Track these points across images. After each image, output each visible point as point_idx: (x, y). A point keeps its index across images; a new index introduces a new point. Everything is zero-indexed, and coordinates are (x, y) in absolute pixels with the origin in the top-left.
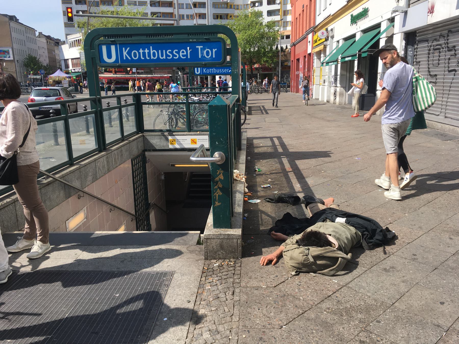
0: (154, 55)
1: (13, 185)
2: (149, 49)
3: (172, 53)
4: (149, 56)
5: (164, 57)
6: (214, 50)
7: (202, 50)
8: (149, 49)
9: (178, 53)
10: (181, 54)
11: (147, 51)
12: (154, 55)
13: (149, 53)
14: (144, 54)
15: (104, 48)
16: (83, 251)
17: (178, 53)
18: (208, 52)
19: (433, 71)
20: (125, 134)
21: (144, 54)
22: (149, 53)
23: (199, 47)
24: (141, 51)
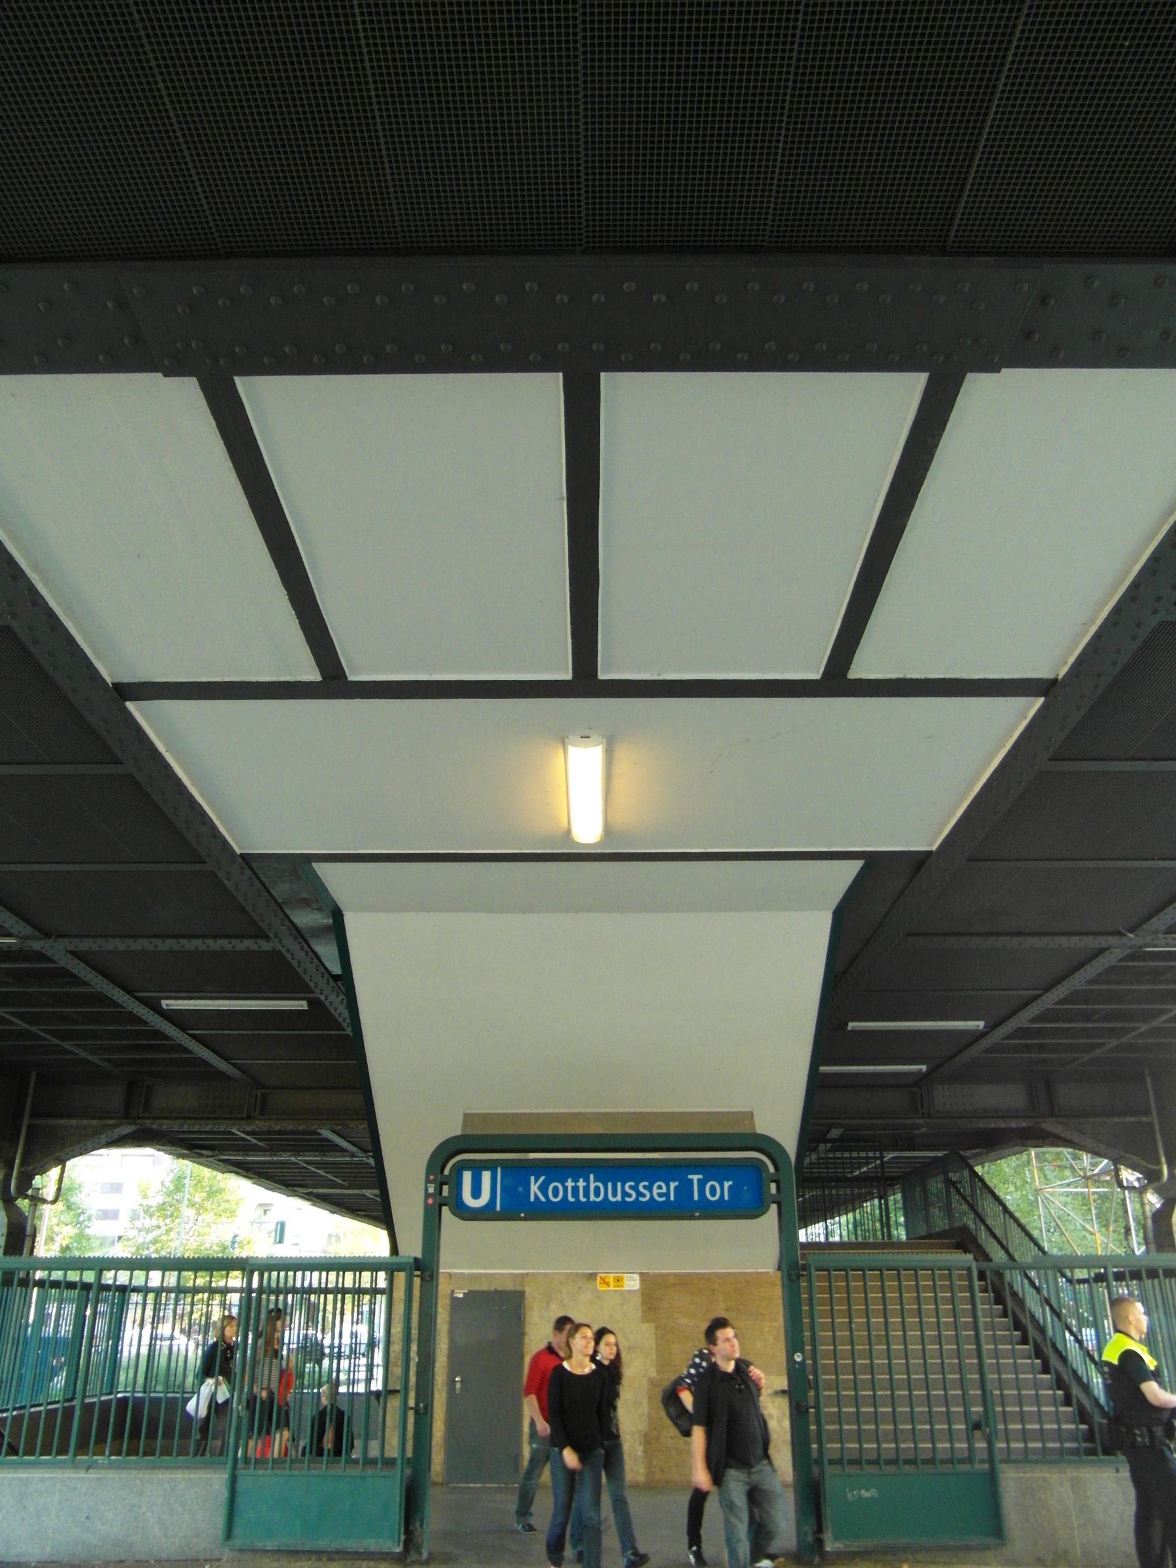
0: (597, 1194)
2: (587, 1180)
3: (640, 1194)
4: (587, 1194)
5: (619, 1198)
6: (727, 1184)
7: (702, 1184)
9: (649, 1188)
10: (655, 1191)
11: (581, 1184)
12: (597, 1194)
13: (587, 1189)
14: (575, 1189)
15: (467, 1176)
17: (649, 1188)
18: (556, 1190)
20: (312, 674)
21: (575, 1189)
22: (587, 1189)
23: (695, 1178)
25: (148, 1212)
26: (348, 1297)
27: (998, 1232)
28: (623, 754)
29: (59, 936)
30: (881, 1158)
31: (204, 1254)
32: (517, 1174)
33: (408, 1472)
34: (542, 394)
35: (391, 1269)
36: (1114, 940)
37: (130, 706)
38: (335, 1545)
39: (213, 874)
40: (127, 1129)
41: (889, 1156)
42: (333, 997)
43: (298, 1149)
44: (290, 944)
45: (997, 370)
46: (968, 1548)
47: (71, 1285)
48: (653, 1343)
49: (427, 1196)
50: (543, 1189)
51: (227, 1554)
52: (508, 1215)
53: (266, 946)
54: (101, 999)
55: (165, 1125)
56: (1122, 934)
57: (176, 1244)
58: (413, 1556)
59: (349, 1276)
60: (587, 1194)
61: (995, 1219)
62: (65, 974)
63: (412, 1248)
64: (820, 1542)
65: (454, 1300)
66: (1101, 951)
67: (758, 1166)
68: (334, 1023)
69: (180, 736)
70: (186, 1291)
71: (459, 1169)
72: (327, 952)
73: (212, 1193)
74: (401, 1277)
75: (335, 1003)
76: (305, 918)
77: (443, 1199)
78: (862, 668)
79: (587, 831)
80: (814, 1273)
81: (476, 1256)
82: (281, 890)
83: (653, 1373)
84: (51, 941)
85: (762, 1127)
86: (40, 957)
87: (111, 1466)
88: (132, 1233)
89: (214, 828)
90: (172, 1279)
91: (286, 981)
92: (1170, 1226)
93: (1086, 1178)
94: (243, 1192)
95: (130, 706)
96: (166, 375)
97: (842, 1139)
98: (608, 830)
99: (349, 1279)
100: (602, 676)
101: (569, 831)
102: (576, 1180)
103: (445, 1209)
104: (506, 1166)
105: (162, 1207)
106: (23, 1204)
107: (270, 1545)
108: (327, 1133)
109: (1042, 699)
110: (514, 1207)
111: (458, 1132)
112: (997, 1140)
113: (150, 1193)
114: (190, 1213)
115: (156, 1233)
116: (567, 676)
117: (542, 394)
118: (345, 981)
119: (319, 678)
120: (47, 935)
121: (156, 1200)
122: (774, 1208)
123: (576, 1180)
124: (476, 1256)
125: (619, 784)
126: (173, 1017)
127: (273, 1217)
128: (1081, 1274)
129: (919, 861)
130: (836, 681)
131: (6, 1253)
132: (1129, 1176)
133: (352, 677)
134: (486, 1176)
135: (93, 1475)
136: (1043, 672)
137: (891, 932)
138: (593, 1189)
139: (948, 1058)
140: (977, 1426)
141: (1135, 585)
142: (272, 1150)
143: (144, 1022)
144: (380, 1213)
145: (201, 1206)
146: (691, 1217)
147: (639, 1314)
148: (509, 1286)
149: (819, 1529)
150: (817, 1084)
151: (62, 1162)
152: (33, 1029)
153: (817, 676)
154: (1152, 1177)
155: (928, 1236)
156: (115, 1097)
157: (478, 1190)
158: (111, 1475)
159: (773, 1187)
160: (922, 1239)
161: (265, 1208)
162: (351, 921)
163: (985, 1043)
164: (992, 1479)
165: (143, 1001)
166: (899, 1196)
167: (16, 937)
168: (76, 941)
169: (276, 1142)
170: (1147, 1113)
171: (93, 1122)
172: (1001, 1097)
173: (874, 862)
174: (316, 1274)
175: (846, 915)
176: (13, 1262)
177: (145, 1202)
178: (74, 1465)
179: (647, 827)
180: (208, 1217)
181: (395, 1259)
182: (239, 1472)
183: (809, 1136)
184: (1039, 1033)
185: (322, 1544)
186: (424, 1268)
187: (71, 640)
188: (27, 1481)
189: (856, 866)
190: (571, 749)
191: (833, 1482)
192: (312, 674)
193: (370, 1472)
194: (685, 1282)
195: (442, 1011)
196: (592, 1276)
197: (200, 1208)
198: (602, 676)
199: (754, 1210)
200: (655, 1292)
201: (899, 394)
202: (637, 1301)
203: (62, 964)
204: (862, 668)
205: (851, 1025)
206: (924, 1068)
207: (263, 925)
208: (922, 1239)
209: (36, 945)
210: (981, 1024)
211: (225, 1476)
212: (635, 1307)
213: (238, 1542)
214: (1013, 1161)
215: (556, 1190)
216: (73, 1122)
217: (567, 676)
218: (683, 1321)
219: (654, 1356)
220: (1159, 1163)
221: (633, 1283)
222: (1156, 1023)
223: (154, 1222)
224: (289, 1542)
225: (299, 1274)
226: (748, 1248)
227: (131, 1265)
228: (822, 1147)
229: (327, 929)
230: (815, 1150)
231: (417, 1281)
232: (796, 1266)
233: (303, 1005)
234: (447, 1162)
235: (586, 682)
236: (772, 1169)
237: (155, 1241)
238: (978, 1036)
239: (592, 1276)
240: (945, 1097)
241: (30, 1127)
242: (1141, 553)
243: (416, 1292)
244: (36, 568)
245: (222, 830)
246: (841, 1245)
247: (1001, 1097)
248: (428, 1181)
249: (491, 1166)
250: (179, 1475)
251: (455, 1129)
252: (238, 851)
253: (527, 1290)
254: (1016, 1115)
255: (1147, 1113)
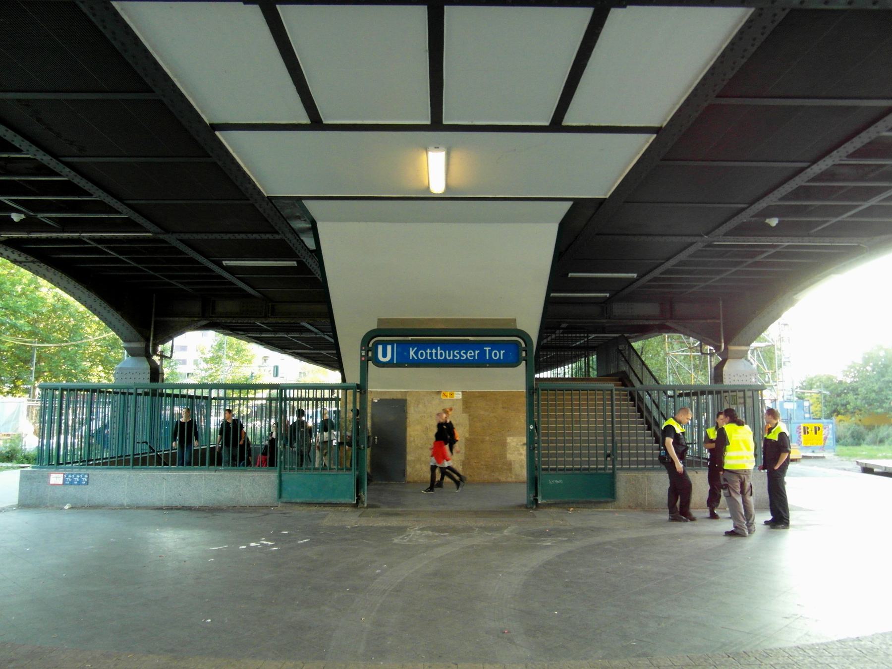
0: (441, 355)
1: (570, 275)
2: (436, 349)
3: (461, 356)
4: (436, 356)
6: (502, 352)
7: (490, 352)
8: (436, 349)
9: (466, 353)
11: (434, 351)
12: (441, 355)
13: (436, 354)
14: (431, 354)
15: (380, 348)
16: (780, 316)
17: (466, 353)
18: (422, 354)
19: (219, 406)
20: (307, 121)
21: (431, 354)
22: (436, 354)
23: (487, 349)
24: (428, 351)
25: (205, 360)
26: (319, 403)
27: (639, 375)
28: (456, 157)
29: (174, 232)
30: (588, 337)
31: (237, 382)
32: (403, 347)
33: (357, 473)
34: (420, 13)
35: (345, 389)
36: (697, 239)
37: (217, 133)
38: (327, 501)
39: (253, 205)
40: (204, 323)
41: (592, 336)
42: (310, 260)
43: (288, 331)
44: (290, 236)
45: (624, 6)
46: (600, 502)
47: (184, 396)
48: (467, 422)
49: (362, 356)
50: (416, 353)
51: (280, 504)
52: (399, 365)
53: (277, 237)
54: (192, 260)
55: (223, 320)
56: (701, 236)
57: (222, 377)
58: (360, 505)
59: (319, 392)
60: (436, 356)
61: (637, 368)
62: (174, 250)
63: (354, 378)
64: (536, 500)
65: (373, 403)
66: (692, 244)
67: (517, 344)
68: (310, 272)
69: (242, 148)
70: (229, 399)
71: (377, 343)
72: (310, 243)
73: (238, 352)
74: (350, 392)
75: (312, 263)
76: (298, 225)
77: (369, 357)
78: (568, 121)
79: (438, 187)
80: (540, 392)
81: (384, 383)
82: (286, 212)
83: (467, 435)
84: (170, 235)
85: (520, 326)
86: (163, 241)
87: (225, 470)
88: (198, 372)
89: (255, 185)
90: (222, 393)
91: (285, 251)
92: (722, 371)
93: (690, 348)
94: (256, 351)
95: (217, 133)
96: (245, 3)
97: (567, 328)
98: (447, 186)
99: (327, 393)
100: (445, 122)
101: (428, 188)
102: (431, 350)
103: (370, 362)
104: (398, 342)
105: (212, 359)
106: (156, 358)
107: (298, 501)
108: (304, 324)
109: (655, 136)
110: (402, 362)
111: (375, 327)
112: (644, 331)
113: (206, 351)
114: (228, 361)
115: (210, 372)
116: (428, 122)
117: (416, 17)
118: (317, 253)
119: (309, 122)
120: (167, 231)
121: (209, 355)
122: (524, 362)
123: (431, 350)
124: (384, 383)
125: (454, 168)
126: (231, 270)
127: (271, 363)
128: (670, 393)
129: (601, 202)
130: (556, 125)
131: (151, 381)
132: (708, 348)
133: (325, 122)
134: (389, 348)
135: (218, 473)
136: (656, 124)
137: (586, 236)
138: (439, 353)
139: (620, 291)
140: (609, 456)
141: (696, 89)
142: (275, 331)
143: (213, 271)
144: (335, 362)
145: (233, 358)
146: (486, 367)
147: (461, 409)
148: (399, 397)
149: (536, 495)
150: (549, 302)
151: (171, 338)
152: (139, 266)
153: (547, 123)
154: (717, 348)
155: (607, 376)
156: (197, 308)
157: (386, 354)
158: (226, 473)
159: (524, 354)
160: (604, 376)
161: (265, 359)
162: (320, 226)
163: (635, 285)
164: (612, 476)
165: (213, 262)
166: (595, 357)
167: (152, 233)
168: (182, 235)
169: (277, 328)
170: (719, 319)
171: (187, 319)
172: (649, 309)
173: (578, 203)
174: (311, 391)
175: (564, 227)
176: (155, 385)
177: (203, 356)
178: (209, 470)
179: (464, 181)
180: (237, 364)
181: (344, 384)
182: (283, 473)
183: (546, 326)
184: (664, 279)
185: (321, 500)
186: (361, 388)
187: (191, 106)
188: (190, 476)
189: (570, 204)
190: (430, 153)
191: (543, 478)
192: (307, 121)
193: (341, 472)
194: (483, 395)
195: (366, 269)
196: (439, 393)
197: (232, 359)
198: (445, 122)
199: (515, 364)
200: (469, 399)
201: (584, 15)
202: (460, 403)
203: (174, 245)
204: (568, 121)
205: (570, 275)
206: (608, 295)
207: (277, 228)
208: (604, 376)
209: (161, 237)
210: (635, 275)
211: (277, 474)
212: (459, 407)
213: (283, 500)
214: (659, 338)
215: (422, 354)
216: (177, 319)
217: (428, 122)
218: (482, 412)
219: (467, 428)
220: (720, 342)
221: (458, 396)
222: (723, 276)
223: (209, 366)
224: (308, 500)
225: (288, 391)
226: (512, 380)
227: (195, 387)
228: (557, 332)
229: (308, 229)
230: (554, 333)
231: (358, 395)
232: (534, 389)
233: (294, 263)
234: (370, 342)
235: (437, 124)
236: (524, 345)
237: (210, 376)
238: (632, 281)
239: (439, 393)
240: (618, 309)
241: (155, 322)
242: (633, 159)
243: (358, 400)
244: (176, 76)
245: (258, 186)
246: (568, 379)
247: (647, 309)
248: (362, 350)
249: (391, 343)
250: (256, 474)
251: (374, 326)
252: (266, 195)
253: (408, 399)
254: (654, 318)
255: (719, 319)
